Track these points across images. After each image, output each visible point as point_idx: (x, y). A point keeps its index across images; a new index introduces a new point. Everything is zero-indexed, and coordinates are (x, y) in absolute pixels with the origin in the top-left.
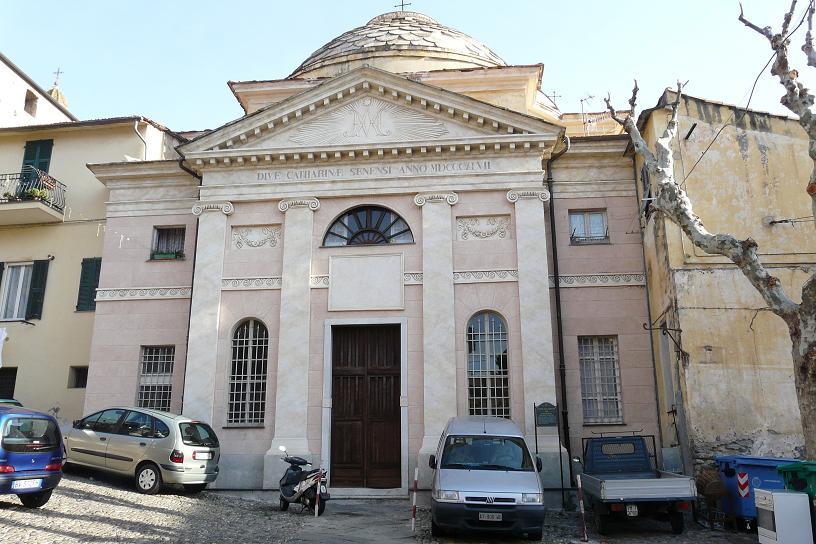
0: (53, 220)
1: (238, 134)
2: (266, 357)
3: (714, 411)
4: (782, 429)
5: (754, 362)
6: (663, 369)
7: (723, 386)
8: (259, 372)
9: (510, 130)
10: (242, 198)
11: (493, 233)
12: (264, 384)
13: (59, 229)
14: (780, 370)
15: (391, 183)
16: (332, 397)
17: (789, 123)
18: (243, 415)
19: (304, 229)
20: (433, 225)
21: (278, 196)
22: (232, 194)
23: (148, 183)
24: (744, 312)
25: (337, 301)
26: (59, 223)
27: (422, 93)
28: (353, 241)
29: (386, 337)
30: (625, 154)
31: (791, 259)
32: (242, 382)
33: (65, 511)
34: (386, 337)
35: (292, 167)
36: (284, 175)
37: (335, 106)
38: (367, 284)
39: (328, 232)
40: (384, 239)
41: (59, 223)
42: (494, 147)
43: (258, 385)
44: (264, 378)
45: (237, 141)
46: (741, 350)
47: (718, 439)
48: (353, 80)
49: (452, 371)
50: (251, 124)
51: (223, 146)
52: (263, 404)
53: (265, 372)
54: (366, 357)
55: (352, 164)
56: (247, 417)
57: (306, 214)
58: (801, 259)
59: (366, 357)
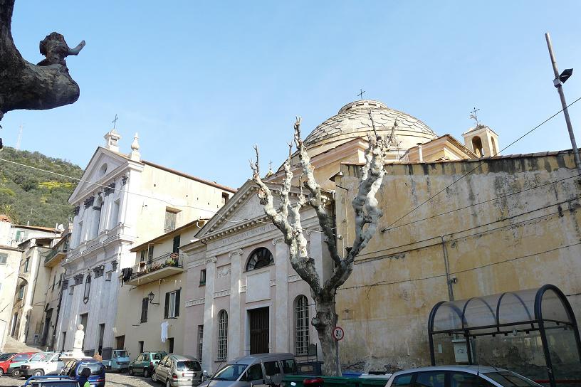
0: (174, 273)
3: (348, 347)
4: (378, 356)
5: (368, 317)
7: (353, 332)
10: (219, 254)
13: (183, 275)
14: (380, 320)
15: (265, 235)
17: (395, 167)
18: (302, 349)
19: (239, 263)
21: (271, 238)
22: (215, 253)
23: (198, 251)
24: (367, 288)
25: (250, 298)
26: (181, 272)
28: (256, 267)
29: (265, 311)
30: (443, 167)
31: (391, 252)
32: (301, 330)
34: (265, 311)
36: (227, 241)
37: (246, 201)
39: (248, 264)
41: (181, 272)
45: (215, 228)
46: (362, 310)
47: (349, 362)
49: (286, 328)
51: (210, 231)
56: (304, 350)
57: (237, 257)
58: (397, 251)
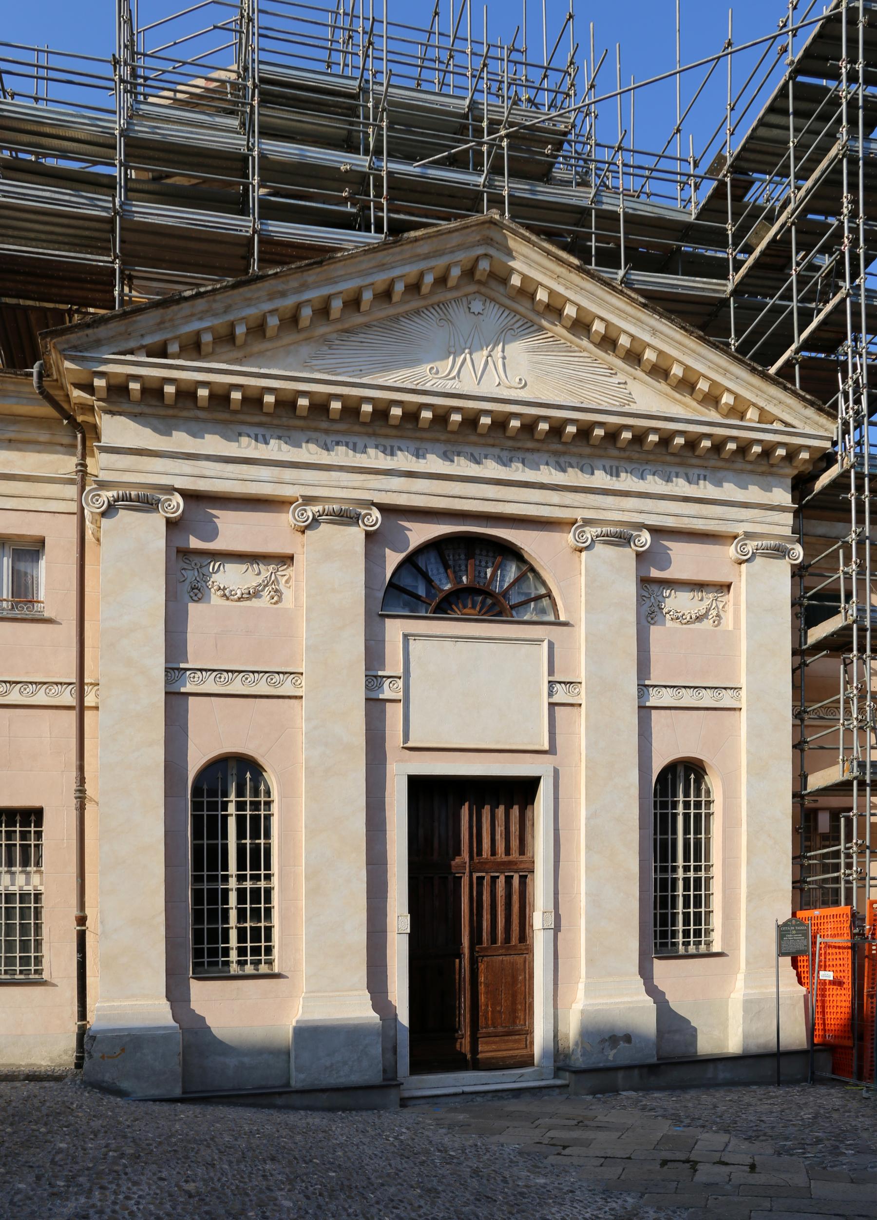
1: (196, 326)
2: (268, 835)
6: (583, 904)
8: (255, 866)
9: (174, 348)
11: (699, 619)
12: (268, 891)
16: (410, 911)
20: (587, 584)
27: (602, 302)
32: (262, 884)
33: (775, 990)
35: (316, 430)
38: (470, 693)
40: (494, 606)
42: (195, 393)
43: (256, 892)
44: (268, 877)
48: (460, 247)
50: (227, 309)
52: (269, 930)
53: (268, 867)
54: (460, 838)
55: (447, 441)
59: (460, 838)
